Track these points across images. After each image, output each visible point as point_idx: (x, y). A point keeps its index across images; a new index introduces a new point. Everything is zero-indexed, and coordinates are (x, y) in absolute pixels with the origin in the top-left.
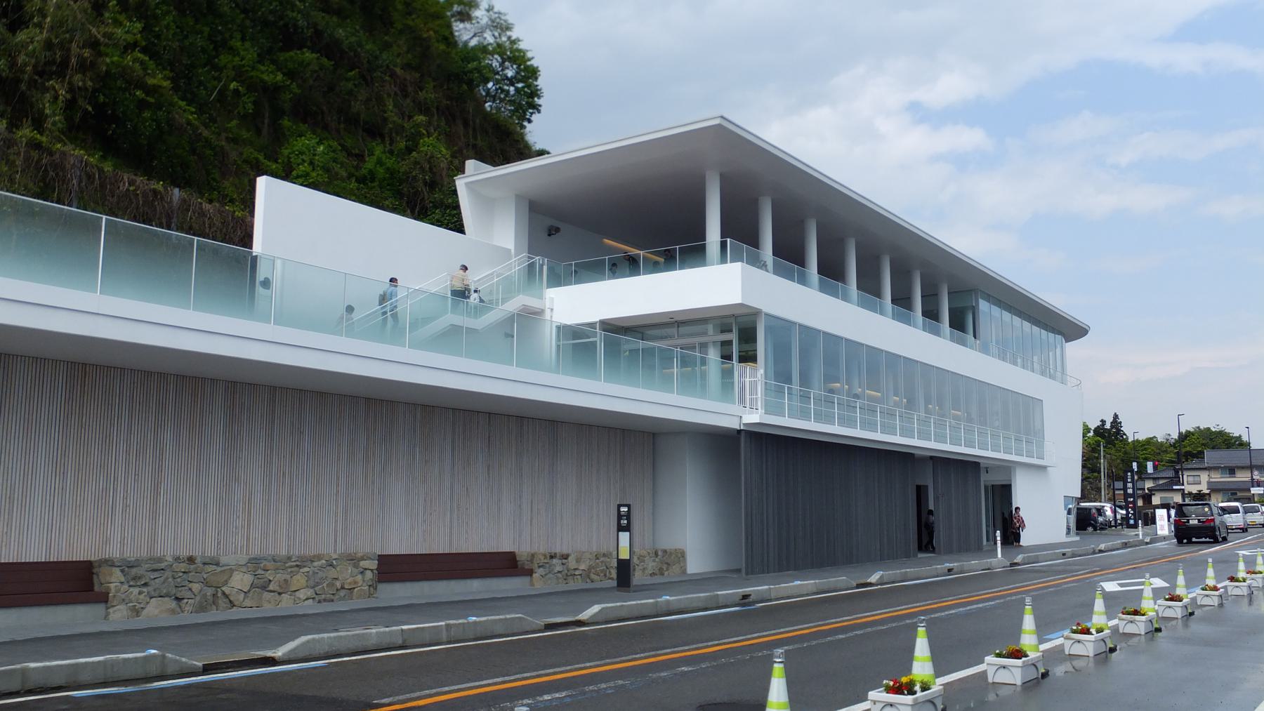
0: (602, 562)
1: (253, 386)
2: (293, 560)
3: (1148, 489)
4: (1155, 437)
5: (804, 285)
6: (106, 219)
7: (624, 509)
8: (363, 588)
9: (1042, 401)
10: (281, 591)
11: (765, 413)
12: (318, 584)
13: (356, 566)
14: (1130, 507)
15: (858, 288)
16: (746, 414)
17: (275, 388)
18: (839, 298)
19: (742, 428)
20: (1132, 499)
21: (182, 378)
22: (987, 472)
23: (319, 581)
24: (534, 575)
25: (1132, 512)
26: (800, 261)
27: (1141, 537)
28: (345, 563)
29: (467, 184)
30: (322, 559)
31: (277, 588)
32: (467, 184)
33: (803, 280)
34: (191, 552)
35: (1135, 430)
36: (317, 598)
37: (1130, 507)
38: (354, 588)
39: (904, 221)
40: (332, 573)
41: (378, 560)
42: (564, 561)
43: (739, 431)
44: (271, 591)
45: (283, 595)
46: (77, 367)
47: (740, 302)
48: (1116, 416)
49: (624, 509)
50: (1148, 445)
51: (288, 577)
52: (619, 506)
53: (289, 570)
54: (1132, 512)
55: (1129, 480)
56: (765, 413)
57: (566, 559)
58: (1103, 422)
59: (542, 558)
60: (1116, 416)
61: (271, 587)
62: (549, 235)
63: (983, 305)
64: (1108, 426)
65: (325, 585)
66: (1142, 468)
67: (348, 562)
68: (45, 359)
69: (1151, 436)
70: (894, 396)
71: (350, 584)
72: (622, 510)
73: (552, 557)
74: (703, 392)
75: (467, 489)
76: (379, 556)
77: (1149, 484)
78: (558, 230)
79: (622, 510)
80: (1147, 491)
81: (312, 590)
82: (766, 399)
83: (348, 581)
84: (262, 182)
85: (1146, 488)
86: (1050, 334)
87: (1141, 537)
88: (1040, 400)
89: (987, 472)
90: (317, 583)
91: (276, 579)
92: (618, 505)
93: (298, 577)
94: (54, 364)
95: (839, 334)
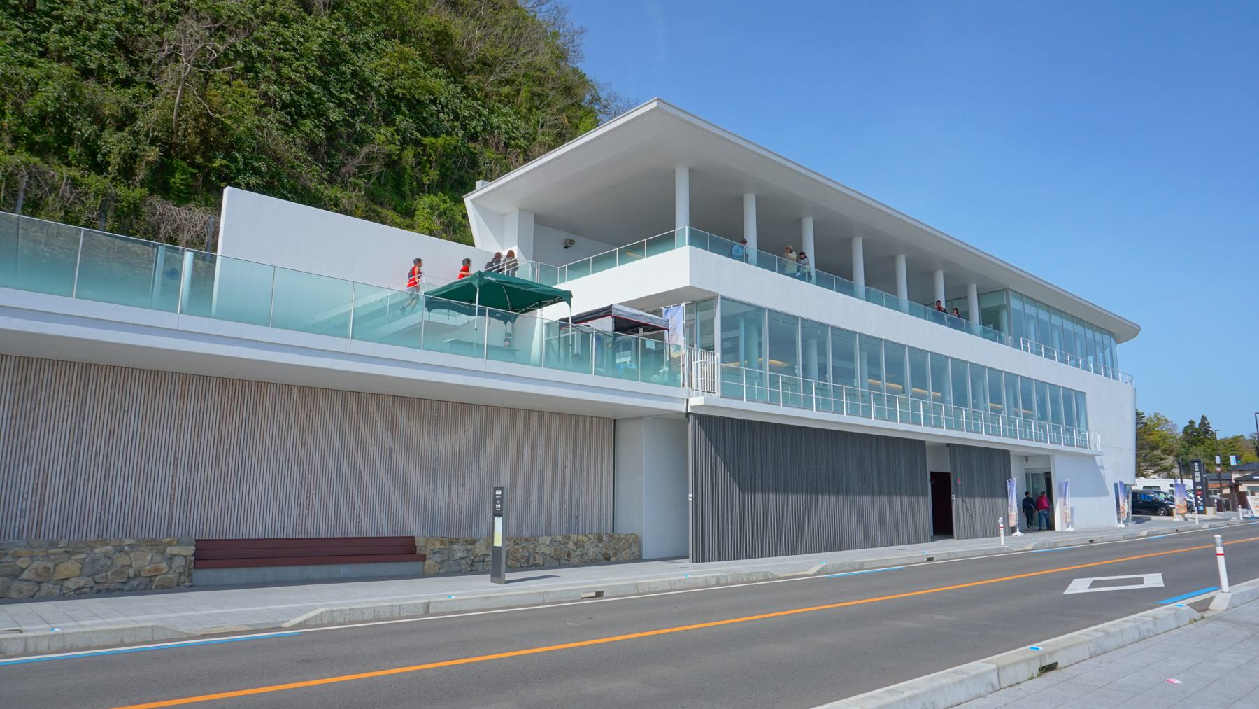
0: (523, 548)
1: (58, 364)
2: (60, 546)
3: (1235, 479)
4: (1242, 436)
5: (853, 296)
6: (489, 310)
7: (499, 492)
8: (169, 576)
9: (1085, 393)
10: (40, 580)
11: (721, 397)
12: (98, 572)
13: (163, 553)
14: (1199, 495)
15: (909, 299)
16: (693, 396)
17: (89, 366)
18: (707, 250)
19: (689, 411)
20: (1200, 487)
21: (225, 382)
22: (1027, 461)
23: (100, 569)
24: (427, 562)
25: (1201, 499)
26: (966, 315)
27: (1197, 523)
28: (144, 549)
29: (472, 201)
30: (108, 545)
31: (33, 576)
32: (472, 201)
33: (895, 306)
34: (221, 536)
35: (1223, 430)
36: (96, 587)
37: (1199, 495)
38: (156, 576)
39: (842, 186)
40: (122, 560)
41: (195, 546)
42: (469, 547)
43: (687, 414)
44: (26, 580)
45: (43, 584)
46: (211, 380)
47: (688, 284)
48: (1204, 418)
49: (499, 492)
50: (1234, 442)
51: (50, 565)
52: (496, 489)
53: (52, 558)
54: (1201, 499)
55: (1197, 470)
56: (721, 397)
57: (471, 544)
58: (1192, 423)
59: (438, 544)
60: (1204, 418)
61: (24, 576)
62: (566, 247)
63: (1015, 304)
64: (1197, 426)
65: (109, 573)
66: (1225, 462)
67: (149, 547)
68: (162, 372)
69: (1239, 435)
70: (869, 378)
71: (149, 571)
72: (497, 493)
73: (452, 543)
74: (169, 300)
75: (360, 473)
76: (196, 540)
77: (1235, 476)
78: (572, 242)
79: (497, 493)
80: (1234, 482)
81: (91, 579)
82: (722, 384)
83: (148, 568)
84: (227, 191)
85: (1233, 478)
86: (1104, 336)
87: (1197, 523)
88: (1082, 392)
89: (1027, 461)
90: (98, 570)
91: (31, 567)
92: (494, 488)
93: (68, 564)
94: (167, 376)
95: (851, 329)
